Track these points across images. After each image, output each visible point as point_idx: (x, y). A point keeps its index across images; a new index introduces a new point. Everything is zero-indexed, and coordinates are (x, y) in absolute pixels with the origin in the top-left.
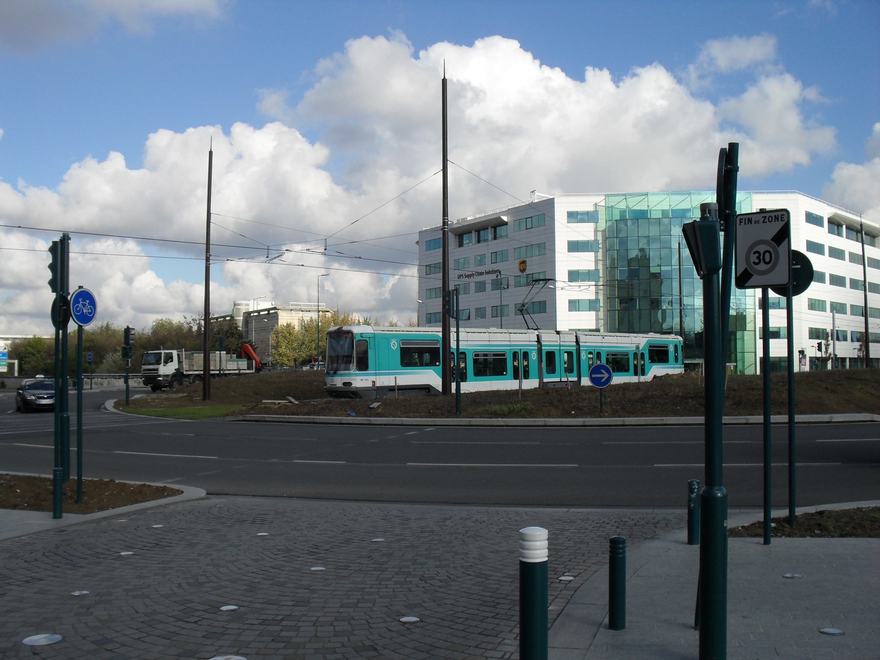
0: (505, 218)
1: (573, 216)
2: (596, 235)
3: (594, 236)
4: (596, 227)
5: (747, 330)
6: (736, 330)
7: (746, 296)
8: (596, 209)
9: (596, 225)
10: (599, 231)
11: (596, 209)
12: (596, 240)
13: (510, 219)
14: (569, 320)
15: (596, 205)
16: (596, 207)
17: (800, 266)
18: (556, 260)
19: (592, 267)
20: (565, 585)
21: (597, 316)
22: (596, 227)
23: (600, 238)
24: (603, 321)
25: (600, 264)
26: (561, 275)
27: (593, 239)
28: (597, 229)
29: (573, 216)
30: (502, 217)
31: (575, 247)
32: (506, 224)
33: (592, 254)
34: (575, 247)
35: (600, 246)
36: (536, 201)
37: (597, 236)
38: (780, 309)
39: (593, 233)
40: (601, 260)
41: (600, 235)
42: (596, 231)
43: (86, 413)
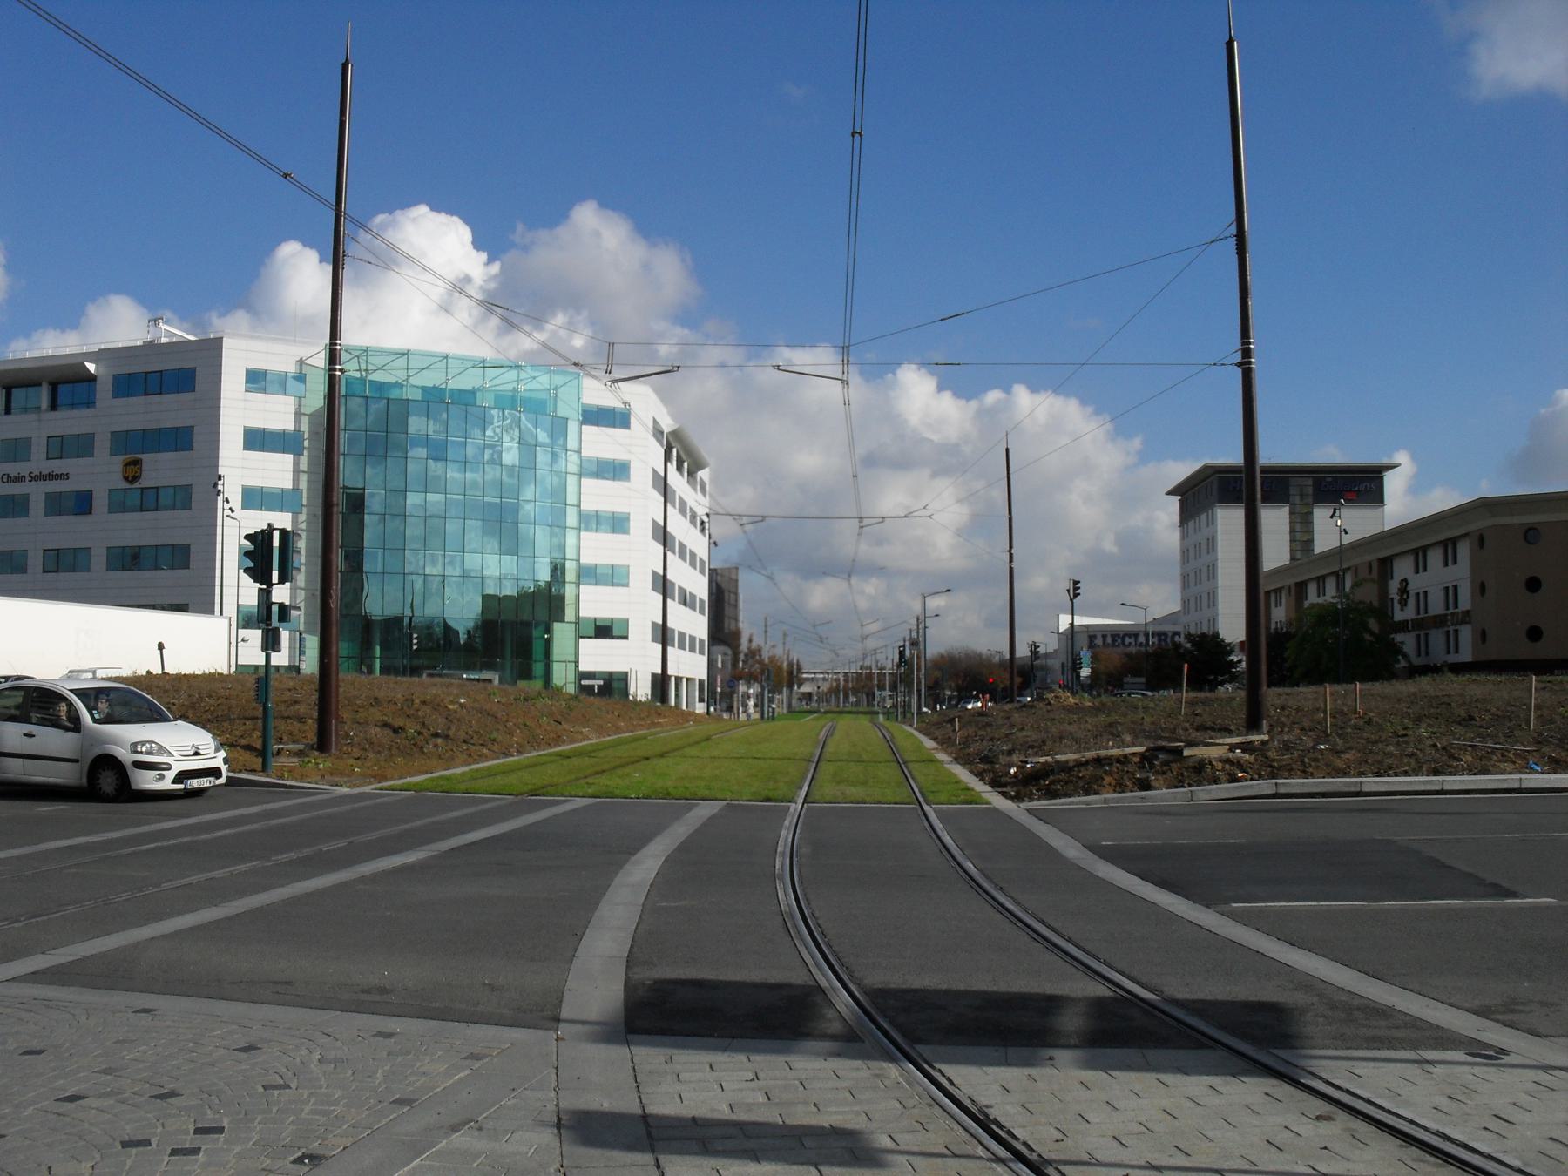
0: (91, 367)
1: (256, 380)
2: (297, 421)
3: (295, 422)
4: (300, 405)
5: (566, 620)
6: (550, 619)
7: (483, 520)
8: (301, 369)
9: (300, 402)
10: (304, 414)
11: (301, 369)
12: (297, 432)
13: (102, 371)
14: (283, 471)
15: (301, 362)
16: (301, 365)
17: (1186, 665)
18: (220, 464)
19: (289, 485)
20: (258, 745)
21: (296, 464)
22: (300, 405)
23: (305, 427)
24: (303, 592)
25: (304, 478)
26: (232, 488)
27: (293, 429)
28: (300, 409)
29: (256, 380)
30: (86, 363)
31: (257, 440)
32: (92, 379)
33: (289, 458)
34: (257, 440)
35: (306, 443)
36: (164, 340)
37: (298, 480)
38: (613, 586)
39: (292, 417)
40: (304, 472)
41: (305, 421)
42: (298, 414)
43: (404, 394)
